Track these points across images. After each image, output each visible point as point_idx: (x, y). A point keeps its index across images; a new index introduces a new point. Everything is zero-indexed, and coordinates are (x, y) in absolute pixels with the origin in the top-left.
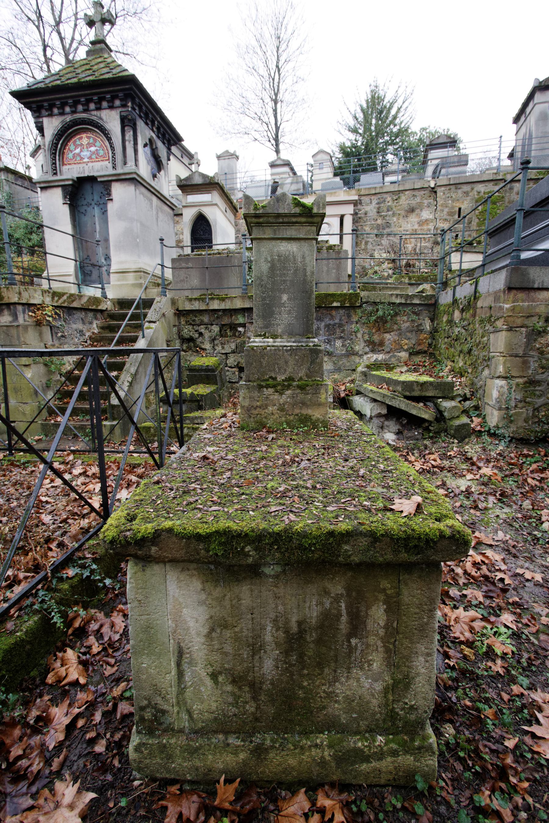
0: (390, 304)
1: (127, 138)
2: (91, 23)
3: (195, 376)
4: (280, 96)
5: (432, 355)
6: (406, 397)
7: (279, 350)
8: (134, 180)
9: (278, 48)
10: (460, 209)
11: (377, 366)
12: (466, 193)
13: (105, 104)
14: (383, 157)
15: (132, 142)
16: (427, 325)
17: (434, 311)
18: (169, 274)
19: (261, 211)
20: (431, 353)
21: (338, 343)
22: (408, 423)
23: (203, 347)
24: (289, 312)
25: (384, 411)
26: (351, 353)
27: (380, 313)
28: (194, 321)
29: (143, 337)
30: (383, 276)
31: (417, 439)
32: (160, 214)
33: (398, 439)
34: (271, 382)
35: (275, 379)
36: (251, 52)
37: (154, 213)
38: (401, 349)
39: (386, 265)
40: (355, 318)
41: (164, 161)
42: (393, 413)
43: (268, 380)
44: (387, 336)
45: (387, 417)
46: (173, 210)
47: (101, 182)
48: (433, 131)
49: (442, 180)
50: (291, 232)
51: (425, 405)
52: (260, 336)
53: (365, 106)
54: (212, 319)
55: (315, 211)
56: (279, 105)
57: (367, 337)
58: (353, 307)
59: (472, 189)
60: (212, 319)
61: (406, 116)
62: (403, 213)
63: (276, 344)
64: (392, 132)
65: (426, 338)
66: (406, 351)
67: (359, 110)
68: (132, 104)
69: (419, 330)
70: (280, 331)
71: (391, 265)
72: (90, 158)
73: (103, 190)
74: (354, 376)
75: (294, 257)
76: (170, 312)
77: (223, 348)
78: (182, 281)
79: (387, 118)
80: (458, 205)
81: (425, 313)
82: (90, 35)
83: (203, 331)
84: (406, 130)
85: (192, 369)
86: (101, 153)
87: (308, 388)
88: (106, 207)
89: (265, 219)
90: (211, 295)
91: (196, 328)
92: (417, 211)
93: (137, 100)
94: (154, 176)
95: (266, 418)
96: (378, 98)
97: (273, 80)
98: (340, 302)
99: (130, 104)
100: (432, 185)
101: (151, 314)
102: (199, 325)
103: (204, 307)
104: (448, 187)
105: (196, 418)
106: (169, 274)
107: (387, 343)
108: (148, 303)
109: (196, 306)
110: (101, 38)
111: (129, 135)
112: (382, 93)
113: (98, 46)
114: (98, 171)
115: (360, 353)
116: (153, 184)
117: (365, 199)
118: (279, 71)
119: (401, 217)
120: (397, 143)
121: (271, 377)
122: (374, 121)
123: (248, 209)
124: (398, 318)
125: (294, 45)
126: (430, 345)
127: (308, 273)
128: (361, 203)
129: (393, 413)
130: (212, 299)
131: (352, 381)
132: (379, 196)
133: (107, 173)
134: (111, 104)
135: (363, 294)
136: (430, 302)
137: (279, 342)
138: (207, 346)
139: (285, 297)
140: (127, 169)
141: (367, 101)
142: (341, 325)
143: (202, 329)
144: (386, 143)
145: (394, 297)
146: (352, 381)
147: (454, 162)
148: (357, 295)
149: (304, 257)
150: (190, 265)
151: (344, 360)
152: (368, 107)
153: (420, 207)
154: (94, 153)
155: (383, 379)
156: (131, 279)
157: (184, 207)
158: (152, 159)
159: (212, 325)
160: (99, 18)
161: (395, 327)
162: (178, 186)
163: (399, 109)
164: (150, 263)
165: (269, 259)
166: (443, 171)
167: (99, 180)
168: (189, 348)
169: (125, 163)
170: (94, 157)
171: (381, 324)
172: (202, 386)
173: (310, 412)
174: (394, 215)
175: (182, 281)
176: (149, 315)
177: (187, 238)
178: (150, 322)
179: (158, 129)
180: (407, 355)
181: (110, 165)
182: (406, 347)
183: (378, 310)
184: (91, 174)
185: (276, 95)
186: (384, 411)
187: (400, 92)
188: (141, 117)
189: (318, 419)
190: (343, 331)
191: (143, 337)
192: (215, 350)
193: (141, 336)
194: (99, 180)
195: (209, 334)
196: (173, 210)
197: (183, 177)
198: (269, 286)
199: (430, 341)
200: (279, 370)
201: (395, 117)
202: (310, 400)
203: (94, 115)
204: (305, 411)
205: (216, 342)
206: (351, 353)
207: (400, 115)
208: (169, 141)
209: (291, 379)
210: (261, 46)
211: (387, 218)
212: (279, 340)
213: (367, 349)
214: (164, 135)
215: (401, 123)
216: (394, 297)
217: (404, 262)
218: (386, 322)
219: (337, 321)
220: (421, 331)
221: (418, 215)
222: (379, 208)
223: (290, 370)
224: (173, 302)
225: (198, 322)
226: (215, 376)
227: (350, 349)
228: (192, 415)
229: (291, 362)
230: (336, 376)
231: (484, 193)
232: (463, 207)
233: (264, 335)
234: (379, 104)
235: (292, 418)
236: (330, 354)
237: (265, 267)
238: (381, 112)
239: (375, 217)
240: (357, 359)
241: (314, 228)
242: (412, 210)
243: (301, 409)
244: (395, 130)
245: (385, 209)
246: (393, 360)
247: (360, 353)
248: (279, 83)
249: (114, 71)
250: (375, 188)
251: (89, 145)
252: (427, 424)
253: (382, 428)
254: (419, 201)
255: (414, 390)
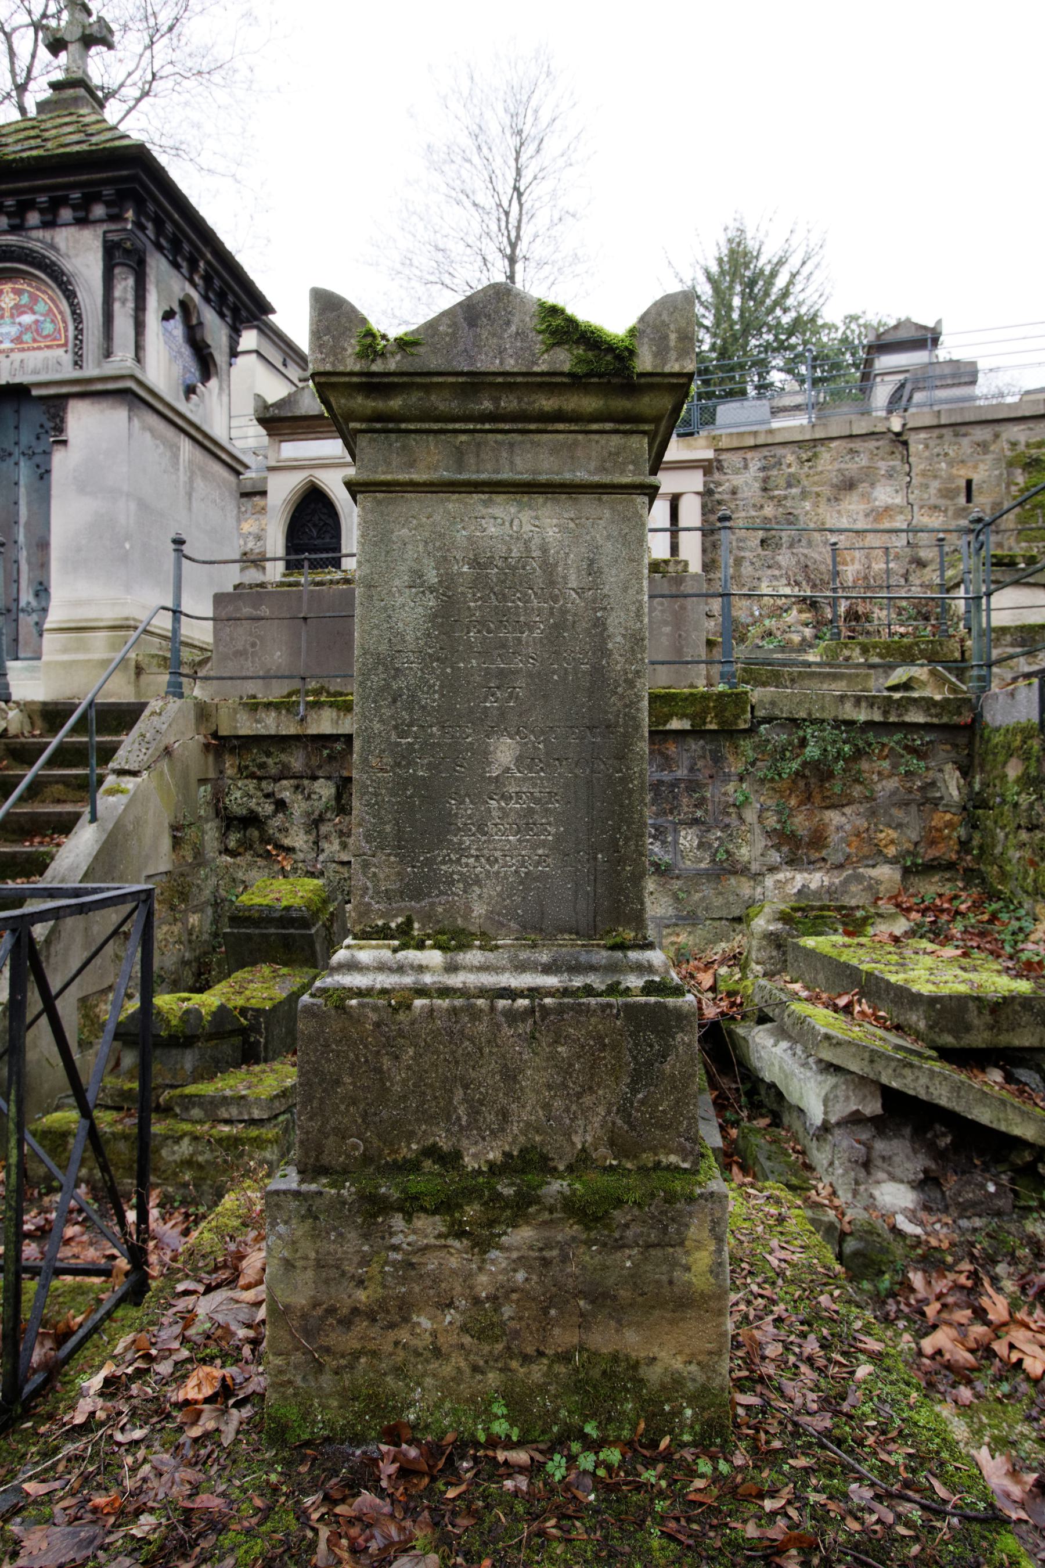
0: (839, 724)
1: (117, 293)
2: (56, 46)
3: (249, 937)
4: (521, 250)
5: (971, 876)
6: (946, 1054)
7: (476, 1015)
8: (131, 395)
9: (518, 153)
10: (969, 483)
11: (807, 915)
12: (983, 446)
13: (66, 214)
14: (760, 375)
15: (131, 305)
16: (952, 786)
17: (970, 744)
18: (200, 632)
19: (392, 365)
20: (967, 870)
21: (688, 839)
22: (955, 1147)
23: (287, 842)
24: (526, 823)
25: (873, 1107)
26: (725, 869)
27: (812, 751)
28: (262, 766)
29: (94, 819)
30: (790, 641)
31: (999, 1214)
32: (199, 483)
33: (927, 1208)
34: (427, 1180)
35: (450, 1159)
36: (458, 160)
37: (183, 477)
38: (877, 856)
39: (793, 616)
40: (735, 766)
41: (220, 357)
42: (902, 1114)
43: (412, 1166)
44: (834, 817)
45: (880, 1125)
46: (238, 473)
47: (41, 398)
48: (875, 323)
49: (919, 416)
50: (535, 458)
51: (1009, 1078)
52: (383, 933)
53: (714, 269)
54: (315, 762)
55: (645, 362)
56: (519, 267)
57: (772, 821)
58: (729, 733)
59: (997, 436)
60: (315, 762)
61: (808, 292)
62: (826, 491)
63: (456, 980)
64: (779, 323)
65: (949, 825)
66: (893, 861)
67: (702, 279)
68: (138, 213)
69: (928, 799)
70: (479, 910)
71: (806, 616)
72: (18, 340)
73: (44, 419)
74: (737, 941)
75: (549, 568)
76: (189, 741)
77: (344, 846)
78: (240, 654)
79: (767, 294)
80: (963, 472)
81: (943, 751)
82: (51, 68)
83: (286, 795)
84: (813, 320)
85: (241, 918)
86: (48, 328)
87: (619, 1216)
88: (49, 462)
89: (414, 399)
90: (317, 692)
91: (268, 786)
92: (863, 487)
93: (151, 207)
94: (190, 390)
95: (399, 1371)
96: (745, 254)
97: (507, 214)
98: (692, 717)
99: (130, 214)
100: (897, 427)
101: (130, 749)
102: (277, 779)
103: (292, 730)
104: (936, 432)
105: (225, 1101)
106: (200, 632)
107: (834, 838)
108: (120, 717)
109: (270, 724)
110: (79, 75)
111: (124, 286)
112: (752, 245)
113: (70, 92)
114: (35, 372)
115: (755, 867)
116: (182, 406)
117: (731, 460)
118: (520, 195)
119: (823, 501)
120: (792, 348)
121: (431, 1152)
122: (737, 302)
123: (336, 351)
124: (865, 765)
125: (553, 146)
126: (964, 846)
127: (617, 642)
128: (720, 469)
129: (902, 1114)
130: (317, 705)
131: (736, 959)
132: (765, 452)
133: (57, 377)
134: (81, 214)
135: (757, 694)
136: (956, 719)
137: (476, 971)
138: (298, 839)
139: (504, 752)
140: (109, 369)
141: (720, 261)
142: (693, 786)
143: (285, 791)
144: (767, 347)
145: (848, 706)
146: (736, 959)
147: (943, 377)
148: (739, 700)
149: (592, 569)
150: (265, 611)
151: (707, 890)
152: (723, 273)
153: (869, 476)
154: (28, 328)
155: (846, 976)
156: (99, 646)
157: (271, 469)
158: (187, 351)
159: (315, 778)
160: (78, 33)
161: (857, 791)
162: (262, 421)
163: (793, 276)
164: (144, 601)
165: (432, 577)
166: (918, 397)
167: (35, 392)
168: (246, 845)
169: (108, 353)
170: (27, 337)
171: (816, 783)
172: (266, 969)
173: (632, 1341)
174: (804, 495)
175: (240, 654)
176: (121, 753)
177: (276, 543)
178: (121, 773)
179: (207, 279)
180: (897, 876)
181: (67, 359)
182: (891, 851)
183: (803, 743)
184: (17, 380)
185: (513, 246)
186: (873, 1107)
187: (794, 243)
188: (159, 248)
189: (678, 1381)
190: (700, 803)
191: (94, 819)
192: (320, 851)
193: (86, 816)
194: (35, 392)
195: (304, 805)
196: (238, 473)
197: (271, 400)
198: (431, 700)
199: (962, 832)
200: (474, 1112)
201: (785, 294)
202: (634, 1278)
203: (36, 239)
204: (604, 1339)
205: (324, 829)
206: (725, 869)
207: (795, 290)
208: (235, 311)
209: (530, 1162)
210: (479, 148)
211: (789, 503)
212: (473, 957)
213: (775, 857)
214: (222, 296)
215: (800, 304)
216: (848, 706)
217: (843, 607)
218: (831, 775)
219: (682, 773)
220: (936, 802)
221: (866, 497)
222: (766, 480)
223: (526, 1112)
224: (203, 713)
225: (273, 771)
226: (310, 940)
227: (721, 856)
228: (206, 1089)
229: (534, 1076)
230: (682, 939)
231: (1028, 445)
232: (976, 478)
233: (405, 930)
234: (747, 267)
235: (537, 1372)
236: (662, 871)
237: (411, 614)
238: (752, 283)
239: (758, 501)
240: (745, 888)
241: (641, 444)
242: (849, 485)
243: (585, 1322)
244: (786, 319)
245: (782, 483)
246: (854, 888)
247: (755, 867)
248: (520, 221)
249: (94, 139)
250: (755, 433)
251: (18, 310)
252: (1028, 1157)
253: (867, 1165)
254: (864, 462)
255: (968, 1028)
